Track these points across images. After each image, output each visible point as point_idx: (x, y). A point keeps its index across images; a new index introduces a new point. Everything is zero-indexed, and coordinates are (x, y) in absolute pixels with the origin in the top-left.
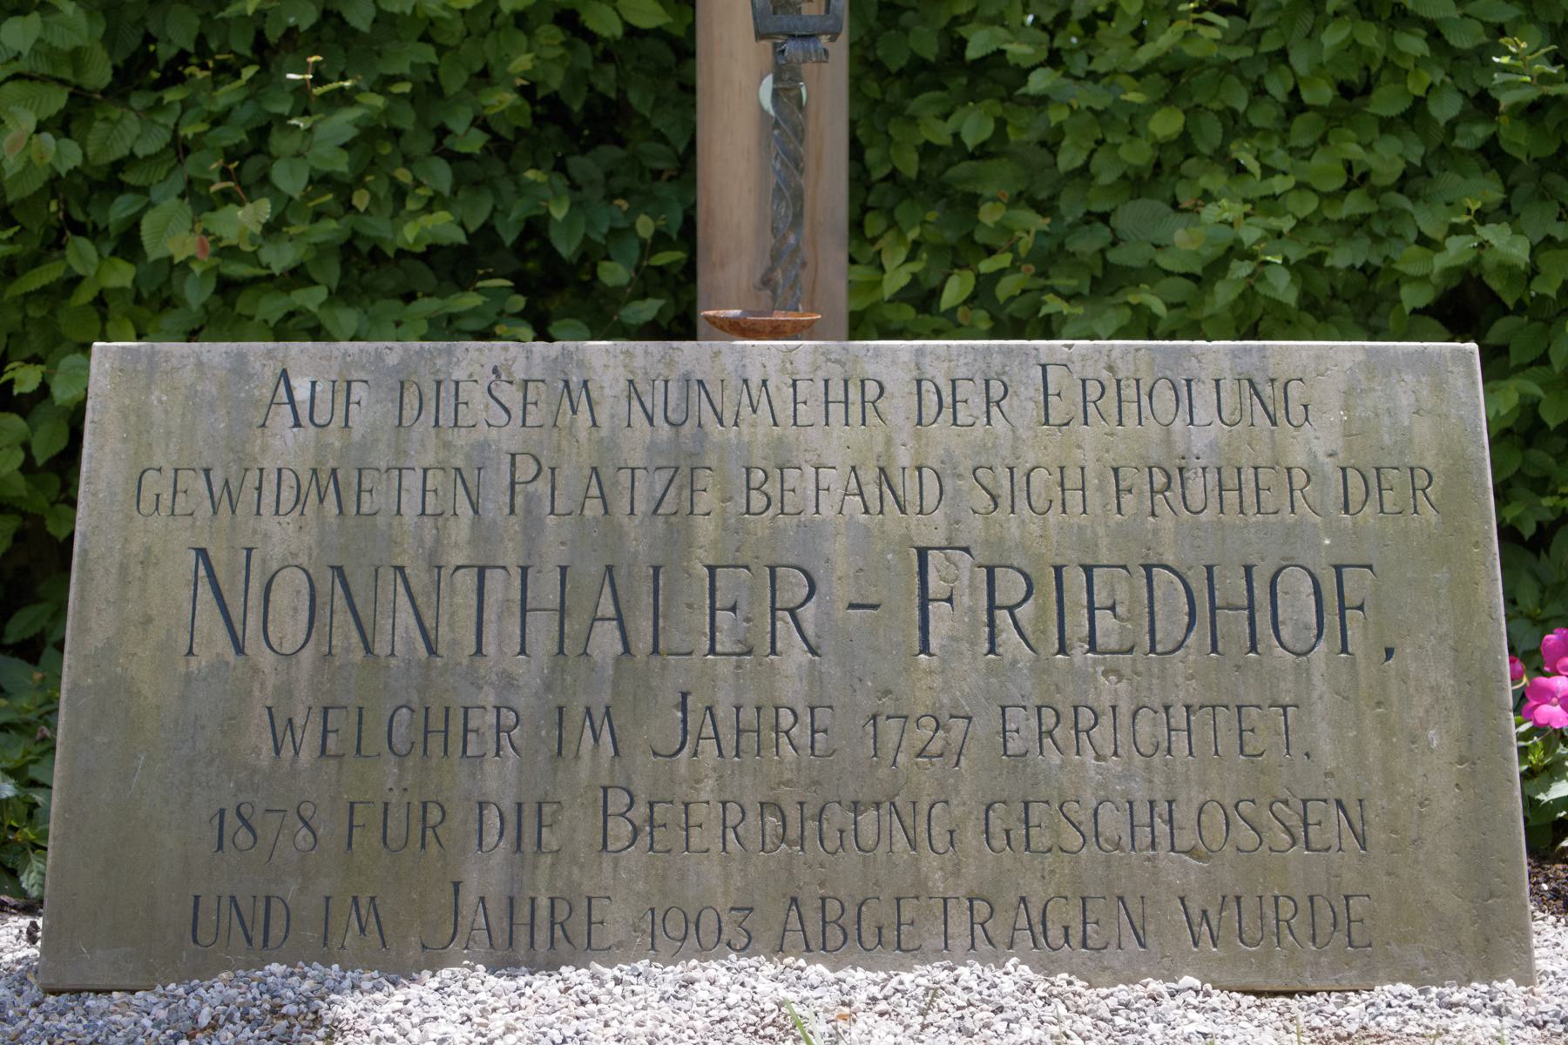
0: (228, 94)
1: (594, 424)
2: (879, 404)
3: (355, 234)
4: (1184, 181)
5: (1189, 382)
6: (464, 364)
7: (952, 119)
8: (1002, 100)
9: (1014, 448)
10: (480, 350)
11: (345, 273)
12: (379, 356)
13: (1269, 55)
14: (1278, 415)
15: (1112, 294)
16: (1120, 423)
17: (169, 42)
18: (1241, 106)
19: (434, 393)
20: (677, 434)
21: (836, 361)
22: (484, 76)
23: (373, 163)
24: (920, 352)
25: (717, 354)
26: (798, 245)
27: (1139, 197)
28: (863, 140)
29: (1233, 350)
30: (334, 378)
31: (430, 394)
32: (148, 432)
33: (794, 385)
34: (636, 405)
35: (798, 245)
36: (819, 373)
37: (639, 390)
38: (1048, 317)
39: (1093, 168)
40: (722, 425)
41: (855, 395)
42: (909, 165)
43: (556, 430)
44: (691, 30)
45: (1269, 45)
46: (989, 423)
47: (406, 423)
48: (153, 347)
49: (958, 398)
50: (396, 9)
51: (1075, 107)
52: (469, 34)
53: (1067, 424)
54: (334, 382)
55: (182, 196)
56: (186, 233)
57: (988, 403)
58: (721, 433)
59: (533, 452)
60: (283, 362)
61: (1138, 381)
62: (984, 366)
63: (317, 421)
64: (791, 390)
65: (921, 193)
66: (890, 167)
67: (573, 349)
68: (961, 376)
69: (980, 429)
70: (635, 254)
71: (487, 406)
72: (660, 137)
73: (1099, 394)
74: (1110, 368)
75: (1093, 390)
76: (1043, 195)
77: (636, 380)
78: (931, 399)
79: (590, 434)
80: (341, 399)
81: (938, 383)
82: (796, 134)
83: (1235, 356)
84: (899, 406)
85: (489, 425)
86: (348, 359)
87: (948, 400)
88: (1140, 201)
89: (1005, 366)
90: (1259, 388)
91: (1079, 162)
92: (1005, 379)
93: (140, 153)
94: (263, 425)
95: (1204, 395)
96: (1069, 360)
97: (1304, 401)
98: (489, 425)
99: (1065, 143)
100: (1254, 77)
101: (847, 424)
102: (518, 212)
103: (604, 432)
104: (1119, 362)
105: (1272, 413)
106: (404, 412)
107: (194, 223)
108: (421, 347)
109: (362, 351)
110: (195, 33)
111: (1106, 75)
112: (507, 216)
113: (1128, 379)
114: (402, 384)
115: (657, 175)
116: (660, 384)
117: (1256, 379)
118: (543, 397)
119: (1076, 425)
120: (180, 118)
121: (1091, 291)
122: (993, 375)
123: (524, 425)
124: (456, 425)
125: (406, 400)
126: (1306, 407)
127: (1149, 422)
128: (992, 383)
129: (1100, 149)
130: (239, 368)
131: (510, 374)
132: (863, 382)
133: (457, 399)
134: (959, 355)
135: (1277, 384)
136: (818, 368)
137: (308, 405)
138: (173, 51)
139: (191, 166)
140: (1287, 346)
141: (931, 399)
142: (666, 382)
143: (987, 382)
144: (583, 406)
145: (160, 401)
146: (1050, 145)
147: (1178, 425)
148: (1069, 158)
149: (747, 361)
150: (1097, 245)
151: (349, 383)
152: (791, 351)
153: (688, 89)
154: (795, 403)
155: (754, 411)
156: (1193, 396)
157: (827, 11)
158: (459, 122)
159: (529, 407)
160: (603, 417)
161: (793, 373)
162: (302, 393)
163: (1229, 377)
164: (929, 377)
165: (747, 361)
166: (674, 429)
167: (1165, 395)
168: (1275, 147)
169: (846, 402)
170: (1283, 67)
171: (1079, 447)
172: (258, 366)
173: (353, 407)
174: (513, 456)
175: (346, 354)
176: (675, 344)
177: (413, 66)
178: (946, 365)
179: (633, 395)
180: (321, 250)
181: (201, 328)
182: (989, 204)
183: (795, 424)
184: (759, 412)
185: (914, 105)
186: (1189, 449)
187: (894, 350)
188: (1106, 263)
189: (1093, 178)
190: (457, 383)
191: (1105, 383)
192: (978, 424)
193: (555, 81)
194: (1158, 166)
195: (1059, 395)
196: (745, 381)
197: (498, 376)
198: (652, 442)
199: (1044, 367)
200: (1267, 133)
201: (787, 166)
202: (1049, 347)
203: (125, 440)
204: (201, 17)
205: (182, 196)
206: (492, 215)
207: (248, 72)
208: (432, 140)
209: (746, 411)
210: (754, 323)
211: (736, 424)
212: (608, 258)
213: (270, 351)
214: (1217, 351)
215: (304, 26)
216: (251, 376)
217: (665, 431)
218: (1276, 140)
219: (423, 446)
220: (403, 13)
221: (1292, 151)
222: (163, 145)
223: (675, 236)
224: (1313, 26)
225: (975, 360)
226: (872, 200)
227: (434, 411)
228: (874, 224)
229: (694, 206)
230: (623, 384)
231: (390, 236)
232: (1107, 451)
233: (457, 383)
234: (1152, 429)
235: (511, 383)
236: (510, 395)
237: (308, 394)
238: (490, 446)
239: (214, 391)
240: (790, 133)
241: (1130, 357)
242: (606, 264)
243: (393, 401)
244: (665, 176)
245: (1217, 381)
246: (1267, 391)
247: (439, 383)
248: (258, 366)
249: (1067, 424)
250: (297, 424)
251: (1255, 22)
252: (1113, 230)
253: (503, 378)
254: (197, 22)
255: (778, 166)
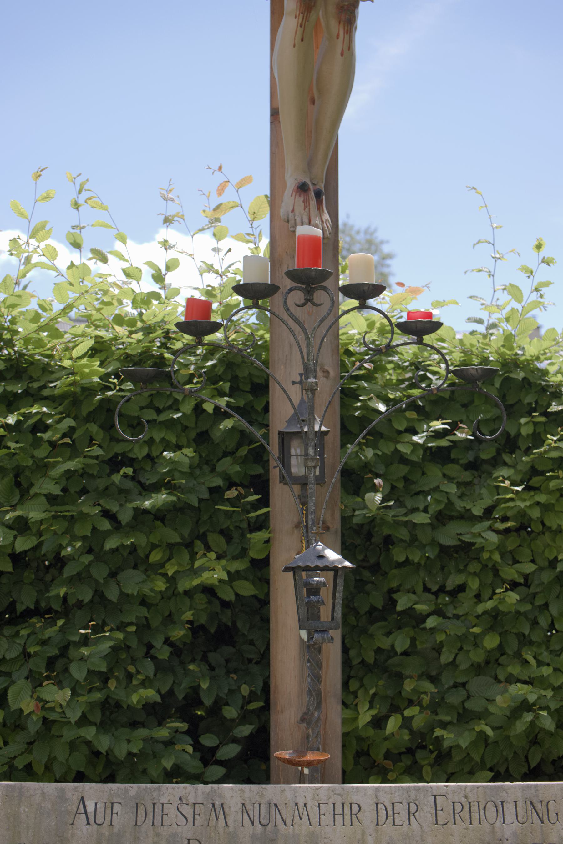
0: (50, 632)
1: (227, 825)
2: (359, 815)
3: (108, 697)
4: (500, 667)
5: (502, 803)
6: (166, 795)
7: (391, 636)
8: (414, 627)
9: (422, 836)
10: (173, 788)
11: (103, 714)
12: (126, 791)
13: (540, 607)
14: (544, 818)
15: (467, 722)
16: (471, 824)
17: (22, 603)
18: (527, 633)
19: (152, 809)
20: (265, 830)
21: (338, 794)
22: (170, 619)
23: (117, 662)
24: (377, 789)
25: (283, 791)
26: (319, 717)
27: (479, 675)
28: (348, 645)
29: (522, 787)
30: (105, 801)
31: (150, 810)
32: (19, 826)
33: (319, 806)
34: (245, 815)
35: (319, 717)
36: (331, 800)
37: (247, 809)
38: (437, 737)
39: (457, 662)
40: (286, 826)
41: (347, 811)
42: (370, 658)
43: (209, 828)
44: (268, 594)
45: (539, 602)
46: (410, 824)
47: (139, 824)
48: (21, 785)
49: (395, 812)
50: (130, 592)
51: (448, 633)
52: (163, 598)
53: (446, 824)
54: (105, 803)
55: (27, 678)
56: (29, 698)
57: (409, 814)
58: (285, 829)
59: (198, 838)
60: (82, 793)
61: (478, 803)
62: (407, 796)
63: (97, 822)
64: (318, 808)
65: (376, 670)
66: (361, 659)
67: (216, 788)
68: (397, 801)
69: (406, 827)
70: (240, 702)
71: (177, 815)
72: (252, 643)
73: (461, 810)
74: (466, 797)
75: (458, 808)
76: (434, 673)
77: (246, 804)
78: (383, 812)
79: (225, 830)
80: (109, 811)
81: (386, 805)
82: (318, 665)
83: (523, 790)
84: (368, 816)
85: (178, 825)
86: (112, 792)
87: (390, 813)
88: (480, 677)
89: (417, 796)
90: (535, 805)
91: (451, 659)
92: (417, 802)
93: (8, 657)
94: (72, 824)
95: (509, 808)
96: (446, 793)
97: (556, 811)
98: (178, 825)
99: (444, 650)
100: (533, 618)
101: (344, 825)
102: (185, 684)
103: (231, 829)
104: (470, 793)
105: (541, 817)
106: (138, 818)
107: (33, 693)
108: (146, 787)
109: (118, 788)
110: (35, 600)
111: (463, 615)
112: (181, 685)
113: (474, 802)
114: (137, 804)
115: (250, 661)
116: (257, 805)
117: (534, 801)
118: (203, 812)
119: (451, 824)
120: (26, 640)
121: (457, 720)
122: (411, 801)
123: (194, 825)
124: (162, 825)
125: (139, 813)
126: (557, 814)
127: (484, 822)
128: (411, 804)
129: (461, 652)
130: (62, 797)
131: (187, 800)
132: (351, 804)
133: (162, 812)
134: (395, 791)
135: (543, 803)
136: (330, 798)
137: (93, 814)
138: (24, 608)
139: (31, 664)
140: (548, 785)
141: (383, 812)
142: (260, 804)
143: (409, 804)
144: (221, 816)
145: (24, 811)
146: (438, 649)
147: (498, 824)
148: (446, 658)
149: (297, 794)
150: (460, 699)
151: (112, 804)
152: (317, 789)
153: (266, 621)
154: (320, 815)
155: (301, 819)
156: (505, 809)
157: (332, 619)
158: (158, 642)
159: (196, 816)
160: (230, 821)
161: (318, 800)
162: (90, 808)
163: (521, 800)
164: (381, 802)
165: (297, 794)
166: (263, 828)
167: (491, 809)
168: (543, 651)
169: (343, 814)
170: (546, 611)
171: (452, 835)
172: (70, 794)
173: (114, 815)
174: (189, 840)
175: (111, 790)
176: (264, 786)
177: (137, 618)
178: (389, 796)
179: (244, 811)
180: (92, 705)
181: (34, 741)
182: (409, 680)
183: (320, 825)
184: (303, 819)
185: (372, 629)
186: (503, 836)
187: (365, 789)
188: (464, 708)
189: (457, 666)
190: (163, 804)
191: (464, 804)
192: (405, 825)
193: (203, 620)
194: (487, 662)
195: (442, 810)
196: (296, 804)
197: (182, 801)
198: (253, 834)
199: (435, 796)
200: (539, 645)
201: (314, 680)
202: (438, 787)
203: (8, 830)
204: (37, 591)
205: (27, 678)
206: (173, 685)
207: (60, 623)
208: (145, 650)
209: (297, 819)
210: (299, 761)
211: (292, 825)
212: (227, 704)
213: (76, 788)
214: (515, 787)
215: (87, 600)
216: (67, 800)
217: (259, 828)
218: (544, 647)
219: (147, 835)
220: (133, 595)
221: (551, 652)
222: (19, 653)
223: (259, 694)
224: (560, 592)
225: (403, 793)
226: (352, 673)
227: (152, 818)
228: (354, 685)
229: (269, 677)
230: (240, 806)
231: (125, 700)
232: (465, 837)
233: (163, 804)
234: (486, 826)
235: (187, 804)
236: (187, 810)
237: (93, 809)
238: (178, 835)
239: (50, 807)
240: (315, 665)
241: (475, 791)
242: (227, 707)
243: (133, 813)
244: (254, 661)
245: (515, 802)
246: (538, 806)
247: (154, 804)
248: (70, 794)
249: (446, 824)
250: (88, 823)
251: (532, 590)
252: (467, 691)
253: (184, 802)
254: (36, 594)
255: (310, 680)
